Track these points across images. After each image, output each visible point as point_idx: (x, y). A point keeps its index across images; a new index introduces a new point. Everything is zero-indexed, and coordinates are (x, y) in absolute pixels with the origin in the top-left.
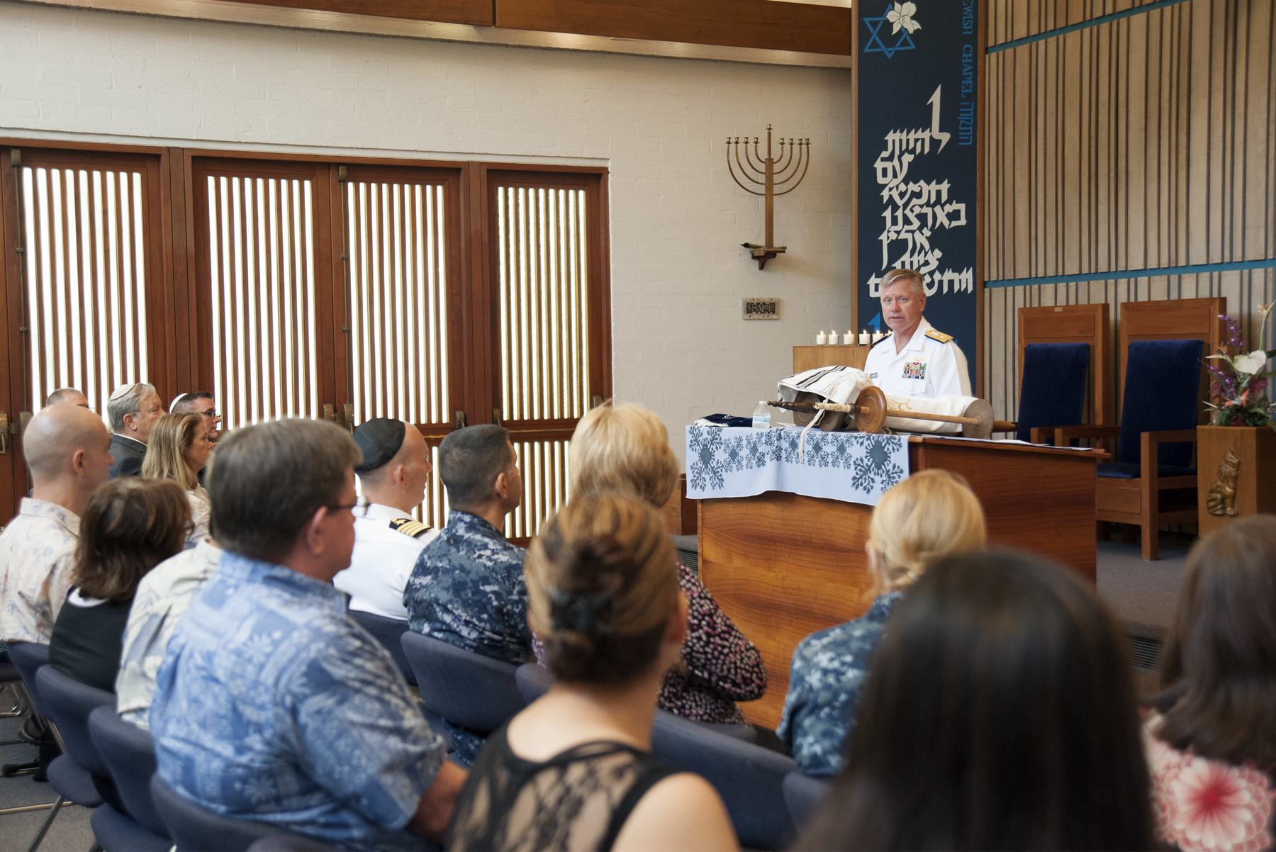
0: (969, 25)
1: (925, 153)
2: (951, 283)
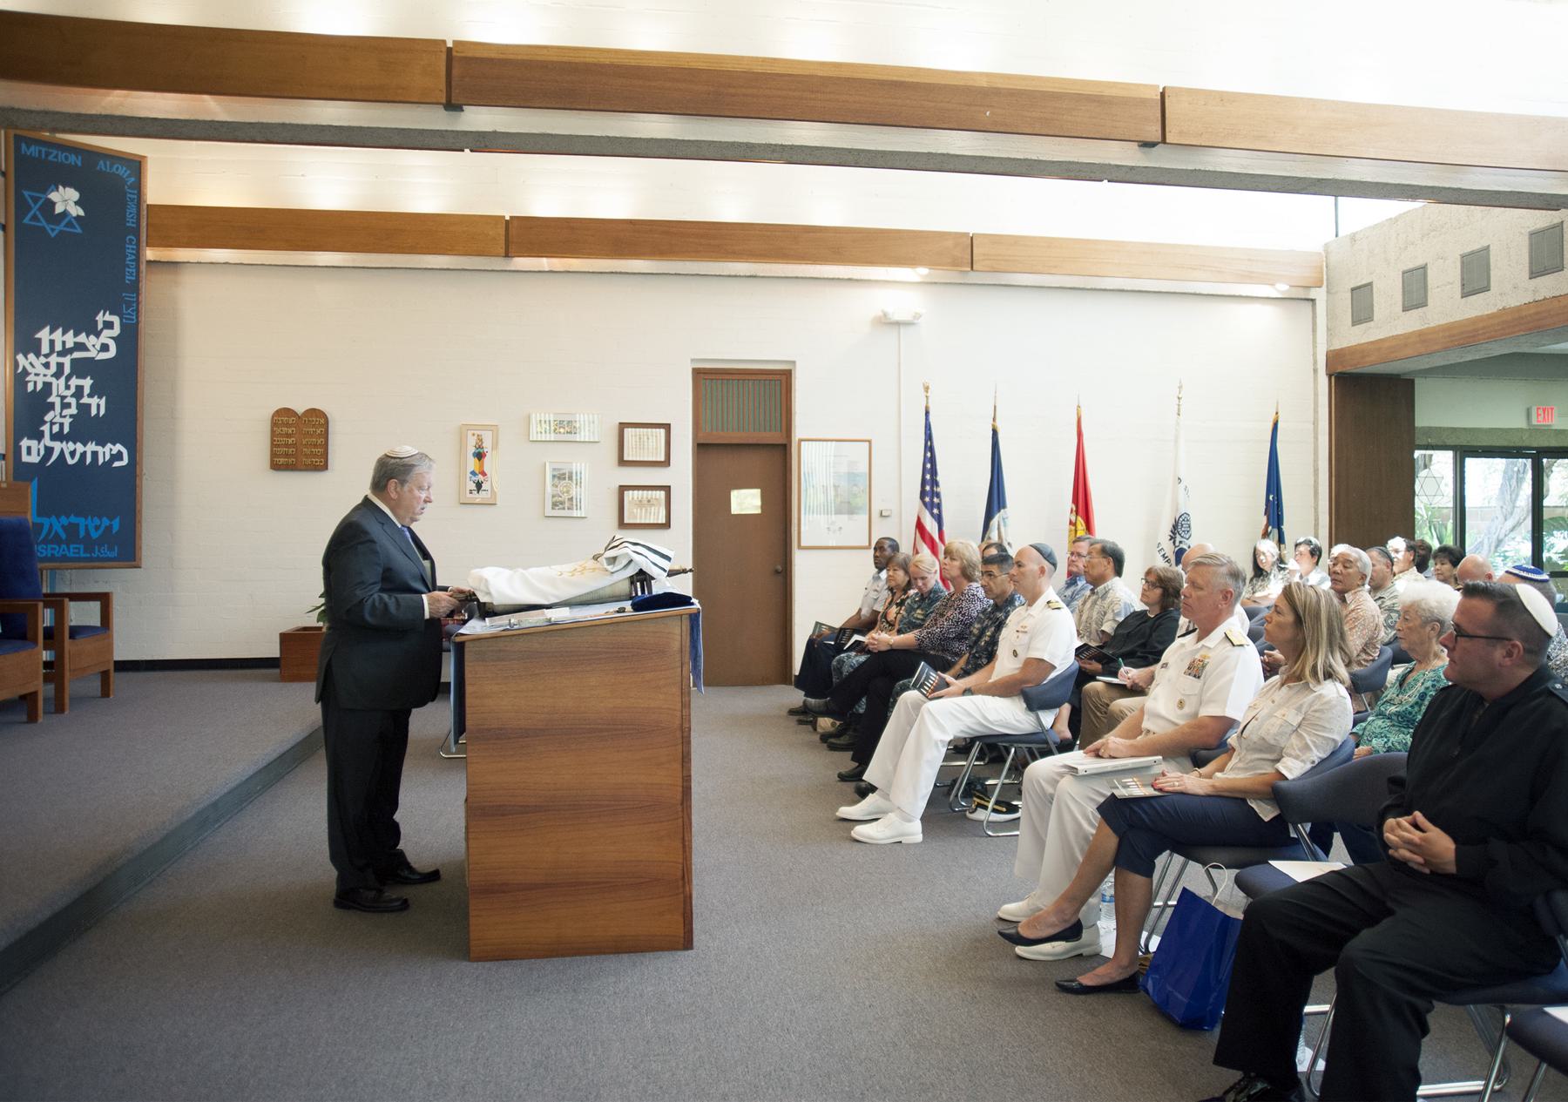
0: (132, 218)
1: (101, 415)
2: (95, 454)
